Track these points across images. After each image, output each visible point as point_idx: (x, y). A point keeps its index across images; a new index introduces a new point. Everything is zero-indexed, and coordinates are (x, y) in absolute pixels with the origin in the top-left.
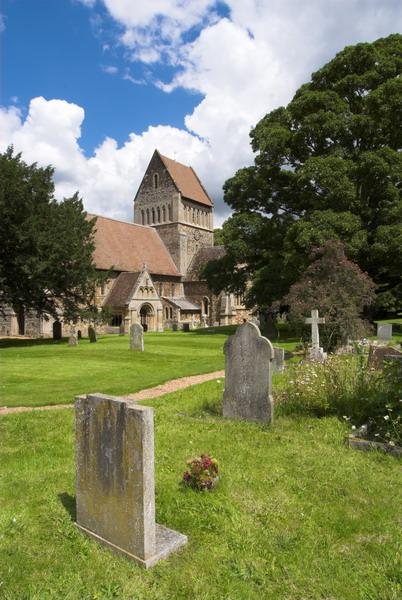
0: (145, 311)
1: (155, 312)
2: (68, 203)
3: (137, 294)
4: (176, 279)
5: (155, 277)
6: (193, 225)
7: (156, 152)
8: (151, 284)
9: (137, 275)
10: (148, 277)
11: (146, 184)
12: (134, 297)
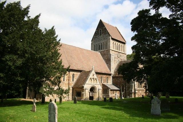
0: (92, 89)
3: (88, 81)
4: (110, 75)
5: (97, 73)
6: (117, 51)
7: (101, 20)
9: (89, 72)
10: (94, 73)
12: (87, 82)
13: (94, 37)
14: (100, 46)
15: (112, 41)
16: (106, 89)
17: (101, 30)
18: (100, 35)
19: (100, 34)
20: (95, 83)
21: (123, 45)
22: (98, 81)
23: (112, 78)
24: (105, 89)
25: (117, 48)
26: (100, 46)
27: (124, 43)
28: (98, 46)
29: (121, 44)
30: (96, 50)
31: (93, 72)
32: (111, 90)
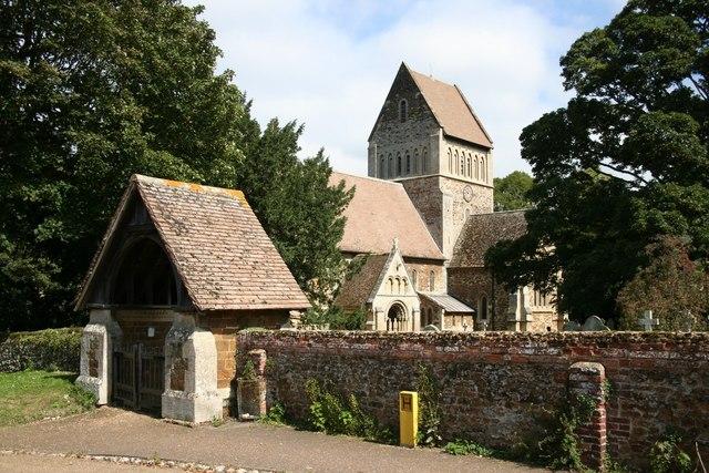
1: (409, 315)
2: (310, 163)
3: (384, 288)
4: (440, 262)
5: (407, 260)
7: (403, 65)
8: (403, 272)
9: (386, 257)
10: (400, 261)
11: (387, 115)
13: (379, 126)
14: (404, 161)
15: (444, 145)
16: (430, 310)
17: (404, 103)
18: (403, 121)
19: (403, 116)
20: (402, 293)
21: (481, 155)
22: (410, 285)
23: (445, 273)
24: (430, 312)
25: (460, 168)
26: (404, 161)
27: (486, 149)
28: (395, 162)
29: (474, 153)
30: (386, 174)
31: (397, 259)
32: (447, 314)
